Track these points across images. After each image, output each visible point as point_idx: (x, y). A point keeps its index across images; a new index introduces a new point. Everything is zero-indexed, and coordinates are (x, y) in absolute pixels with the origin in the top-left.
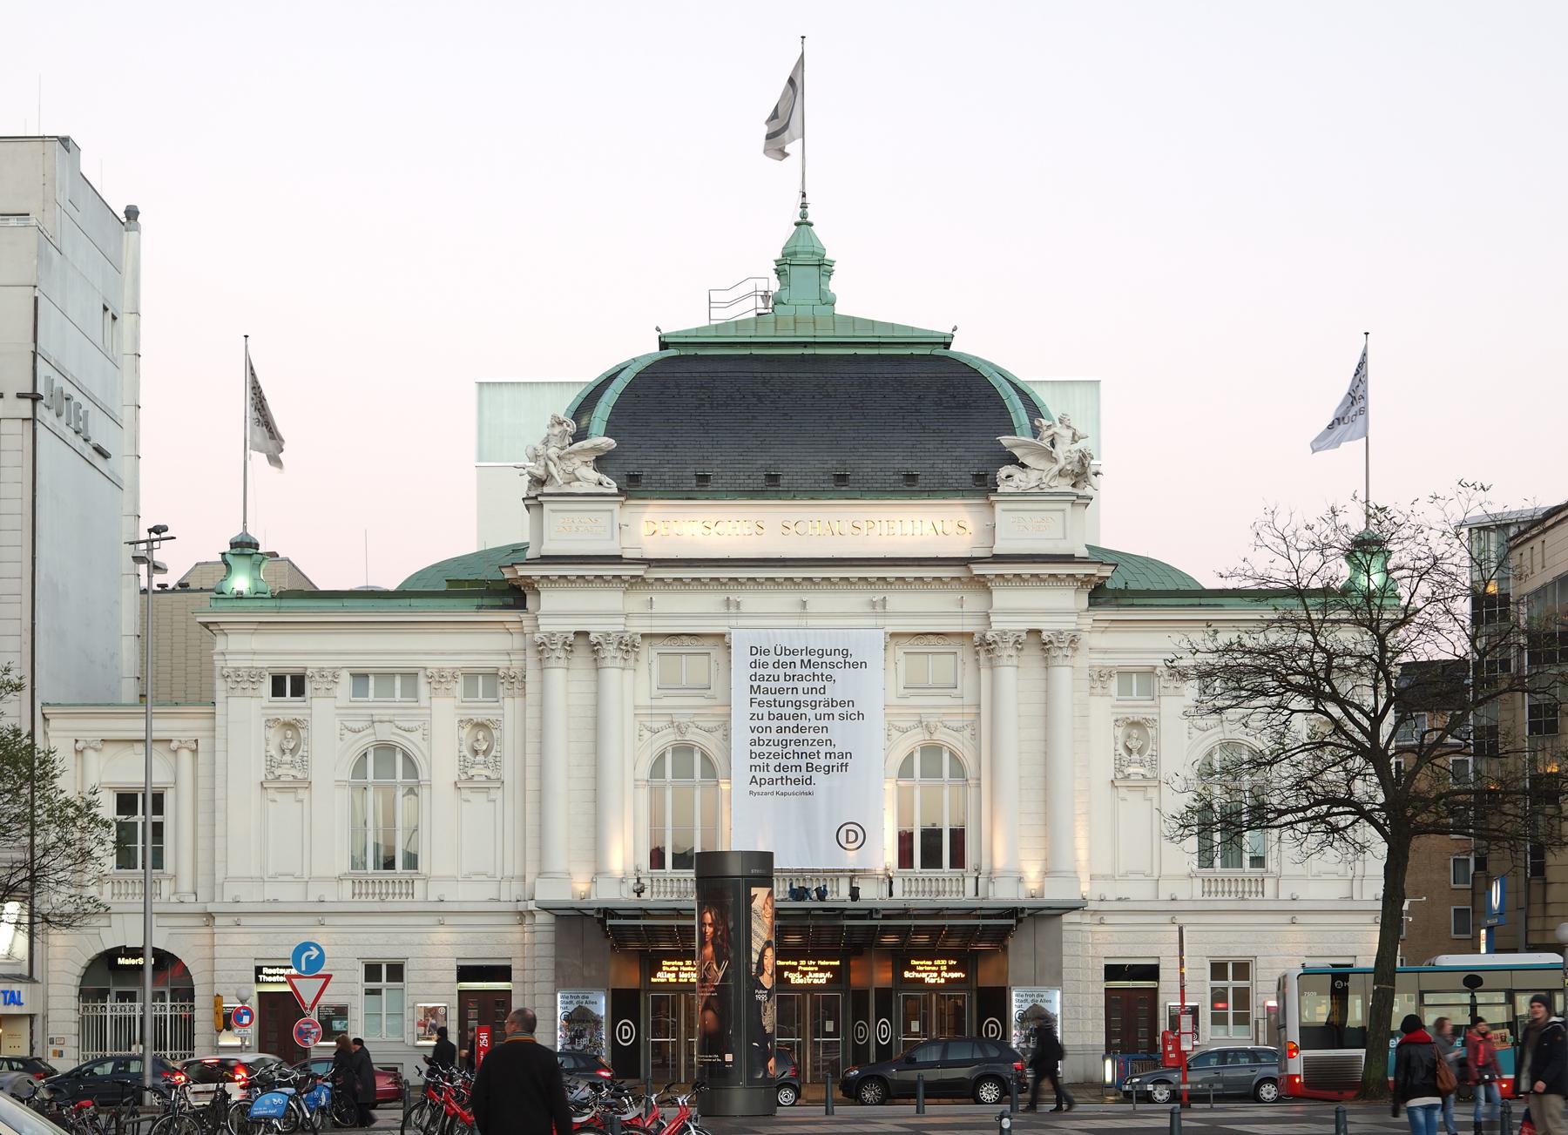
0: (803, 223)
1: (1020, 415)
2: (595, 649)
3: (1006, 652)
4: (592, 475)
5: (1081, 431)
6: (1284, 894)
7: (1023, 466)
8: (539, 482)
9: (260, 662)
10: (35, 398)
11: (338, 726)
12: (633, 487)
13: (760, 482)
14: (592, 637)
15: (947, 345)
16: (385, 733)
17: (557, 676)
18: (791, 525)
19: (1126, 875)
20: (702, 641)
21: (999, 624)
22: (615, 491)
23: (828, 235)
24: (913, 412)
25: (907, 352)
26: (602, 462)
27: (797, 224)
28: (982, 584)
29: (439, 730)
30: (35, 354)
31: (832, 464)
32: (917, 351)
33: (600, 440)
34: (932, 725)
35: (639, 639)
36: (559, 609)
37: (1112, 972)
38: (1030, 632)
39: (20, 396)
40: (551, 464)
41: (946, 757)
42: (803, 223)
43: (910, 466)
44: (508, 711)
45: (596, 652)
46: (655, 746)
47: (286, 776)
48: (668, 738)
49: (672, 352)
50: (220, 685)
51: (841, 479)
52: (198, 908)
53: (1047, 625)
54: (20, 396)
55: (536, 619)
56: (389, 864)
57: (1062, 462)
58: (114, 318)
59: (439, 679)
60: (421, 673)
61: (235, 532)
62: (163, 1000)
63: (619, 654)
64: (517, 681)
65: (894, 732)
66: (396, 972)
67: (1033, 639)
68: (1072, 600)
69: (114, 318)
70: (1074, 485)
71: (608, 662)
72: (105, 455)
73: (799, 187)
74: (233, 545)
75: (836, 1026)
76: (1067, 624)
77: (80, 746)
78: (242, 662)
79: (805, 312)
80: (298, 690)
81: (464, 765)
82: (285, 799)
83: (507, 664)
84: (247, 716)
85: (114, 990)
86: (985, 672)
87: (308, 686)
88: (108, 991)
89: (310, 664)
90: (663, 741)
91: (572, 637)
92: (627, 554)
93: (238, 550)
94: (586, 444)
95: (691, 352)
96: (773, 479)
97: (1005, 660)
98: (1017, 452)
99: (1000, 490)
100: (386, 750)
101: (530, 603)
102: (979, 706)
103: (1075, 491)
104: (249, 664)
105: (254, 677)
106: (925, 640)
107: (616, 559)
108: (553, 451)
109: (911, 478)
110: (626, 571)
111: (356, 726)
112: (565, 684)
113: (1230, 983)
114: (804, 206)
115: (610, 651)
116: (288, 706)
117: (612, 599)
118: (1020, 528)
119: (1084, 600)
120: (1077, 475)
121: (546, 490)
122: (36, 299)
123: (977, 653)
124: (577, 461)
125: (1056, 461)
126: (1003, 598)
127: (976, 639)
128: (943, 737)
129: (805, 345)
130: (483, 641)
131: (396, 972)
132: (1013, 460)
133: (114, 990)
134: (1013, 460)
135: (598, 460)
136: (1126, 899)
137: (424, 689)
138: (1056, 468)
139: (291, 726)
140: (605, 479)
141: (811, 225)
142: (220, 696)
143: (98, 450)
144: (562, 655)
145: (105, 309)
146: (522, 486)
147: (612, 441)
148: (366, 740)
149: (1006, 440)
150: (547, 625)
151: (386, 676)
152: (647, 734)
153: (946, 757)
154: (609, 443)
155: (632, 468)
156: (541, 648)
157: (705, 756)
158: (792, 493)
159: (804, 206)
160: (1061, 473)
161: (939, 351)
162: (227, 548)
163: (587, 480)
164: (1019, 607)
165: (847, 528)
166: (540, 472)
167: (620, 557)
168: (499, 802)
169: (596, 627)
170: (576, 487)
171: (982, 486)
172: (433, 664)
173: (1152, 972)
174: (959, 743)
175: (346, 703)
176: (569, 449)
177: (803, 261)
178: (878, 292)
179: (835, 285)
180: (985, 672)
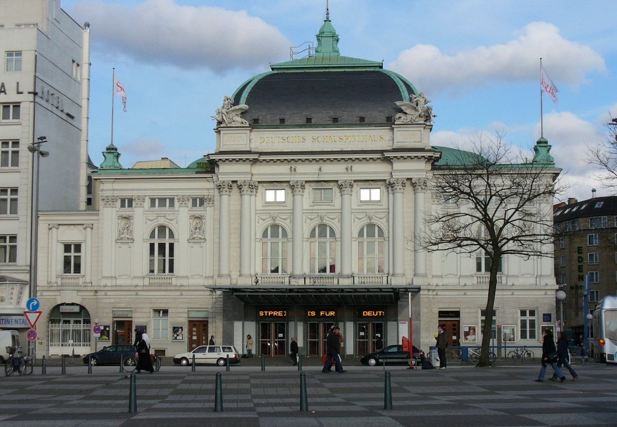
0: (327, 20)
1: (405, 93)
2: (240, 187)
3: (398, 187)
4: (239, 119)
5: (428, 99)
6: (510, 283)
7: (406, 113)
8: (220, 123)
9: (116, 193)
10: (35, 94)
11: (145, 218)
12: (255, 124)
13: (278, 122)
14: (339, 183)
15: (381, 67)
16: (162, 221)
17: (225, 198)
18: (316, 138)
19: (523, 275)
20: (377, 183)
21: (396, 175)
22: (248, 125)
23: (337, 25)
24: (361, 92)
25: (365, 70)
26: (244, 114)
27: (325, 21)
28: (388, 160)
29: (181, 221)
30: (35, 77)
31: (332, 114)
32: (368, 70)
33: (243, 105)
34: (371, 217)
35: (257, 184)
36: (226, 172)
37: (442, 314)
38: (408, 179)
39: (29, 93)
40: (224, 115)
41: (280, 229)
42: (327, 20)
43: (362, 114)
44: (208, 212)
45: (240, 189)
46: (312, 225)
47: (125, 238)
48: (366, 221)
49: (275, 72)
50: (101, 203)
51: (335, 120)
52: (92, 288)
53: (415, 176)
54: (29, 93)
55: (218, 176)
56: (324, 270)
57: (420, 111)
58: (78, 65)
59: (183, 200)
60: (176, 198)
61: (108, 144)
62: (80, 323)
63: (249, 190)
64: (211, 200)
65: (147, 220)
66: (166, 312)
67: (408, 182)
68: (423, 166)
69: (78, 65)
70: (425, 121)
71: (245, 192)
72: (72, 117)
73: (326, 7)
74: (107, 149)
75: (284, 335)
76: (422, 175)
77: (50, 227)
78: (109, 194)
79: (327, 55)
80: (130, 205)
81: (192, 233)
82: (197, 246)
83: (112, 194)
84: (109, 215)
85: (62, 319)
86: (391, 196)
87: (134, 203)
88: (60, 320)
89: (134, 194)
90: (314, 223)
91: (231, 183)
92: (253, 150)
93: (109, 151)
94: (237, 107)
95: (282, 71)
96: (282, 121)
97: (398, 190)
98: (403, 108)
99: (396, 123)
100: (162, 229)
101: (216, 170)
102: (389, 209)
103: (425, 123)
104: (138, 194)
105: (114, 200)
106: (368, 183)
107: (249, 152)
108: (224, 111)
109: (362, 119)
110: (251, 157)
111: (151, 218)
112: (230, 201)
113: (528, 318)
114: (328, 14)
115: (245, 188)
116: (126, 211)
117: (246, 168)
118: (404, 137)
119: (429, 167)
120: (427, 117)
121: (222, 125)
122: (36, 56)
123: (388, 188)
124: (234, 114)
125: (418, 111)
126: (397, 165)
127: (387, 182)
128: (375, 221)
129: (326, 68)
130: (202, 186)
131: (166, 312)
132: (401, 111)
133: (62, 319)
134: (401, 111)
135: (242, 113)
136: (446, 285)
137: (176, 204)
138: (418, 114)
139: (199, 218)
140: (244, 121)
141: (330, 21)
142: (101, 208)
143: (68, 115)
144: (228, 190)
145: (74, 61)
146: (214, 124)
147: (247, 106)
148: (155, 224)
149: (398, 103)
150: (222, 178)
151: (162, 201)
152: (308, 221)
153: (280, 229)
154: (247, 107)
155: (255, 117)
156: (219, 187)
157: (283, 229)
158: (316, 126)
159: (328, 14)
160: (420, 116)
161: (377, 69)
162: (105, 150)
163: (237, 121)
164: (404, 169)
165: (337, 139)
166: (220, 119)
167: (424, 149)
168: (204, 247)
169: (240, 179)
170: (233, 125)
171: (389, 122)
172: (181, 193)
173: (457, 314)
174: (383, 224)
175: (147, 209)
176: (231, 109)
177: (327, 35)
178: (358, 48)
179: (340, 46)
180: (391, 196)
